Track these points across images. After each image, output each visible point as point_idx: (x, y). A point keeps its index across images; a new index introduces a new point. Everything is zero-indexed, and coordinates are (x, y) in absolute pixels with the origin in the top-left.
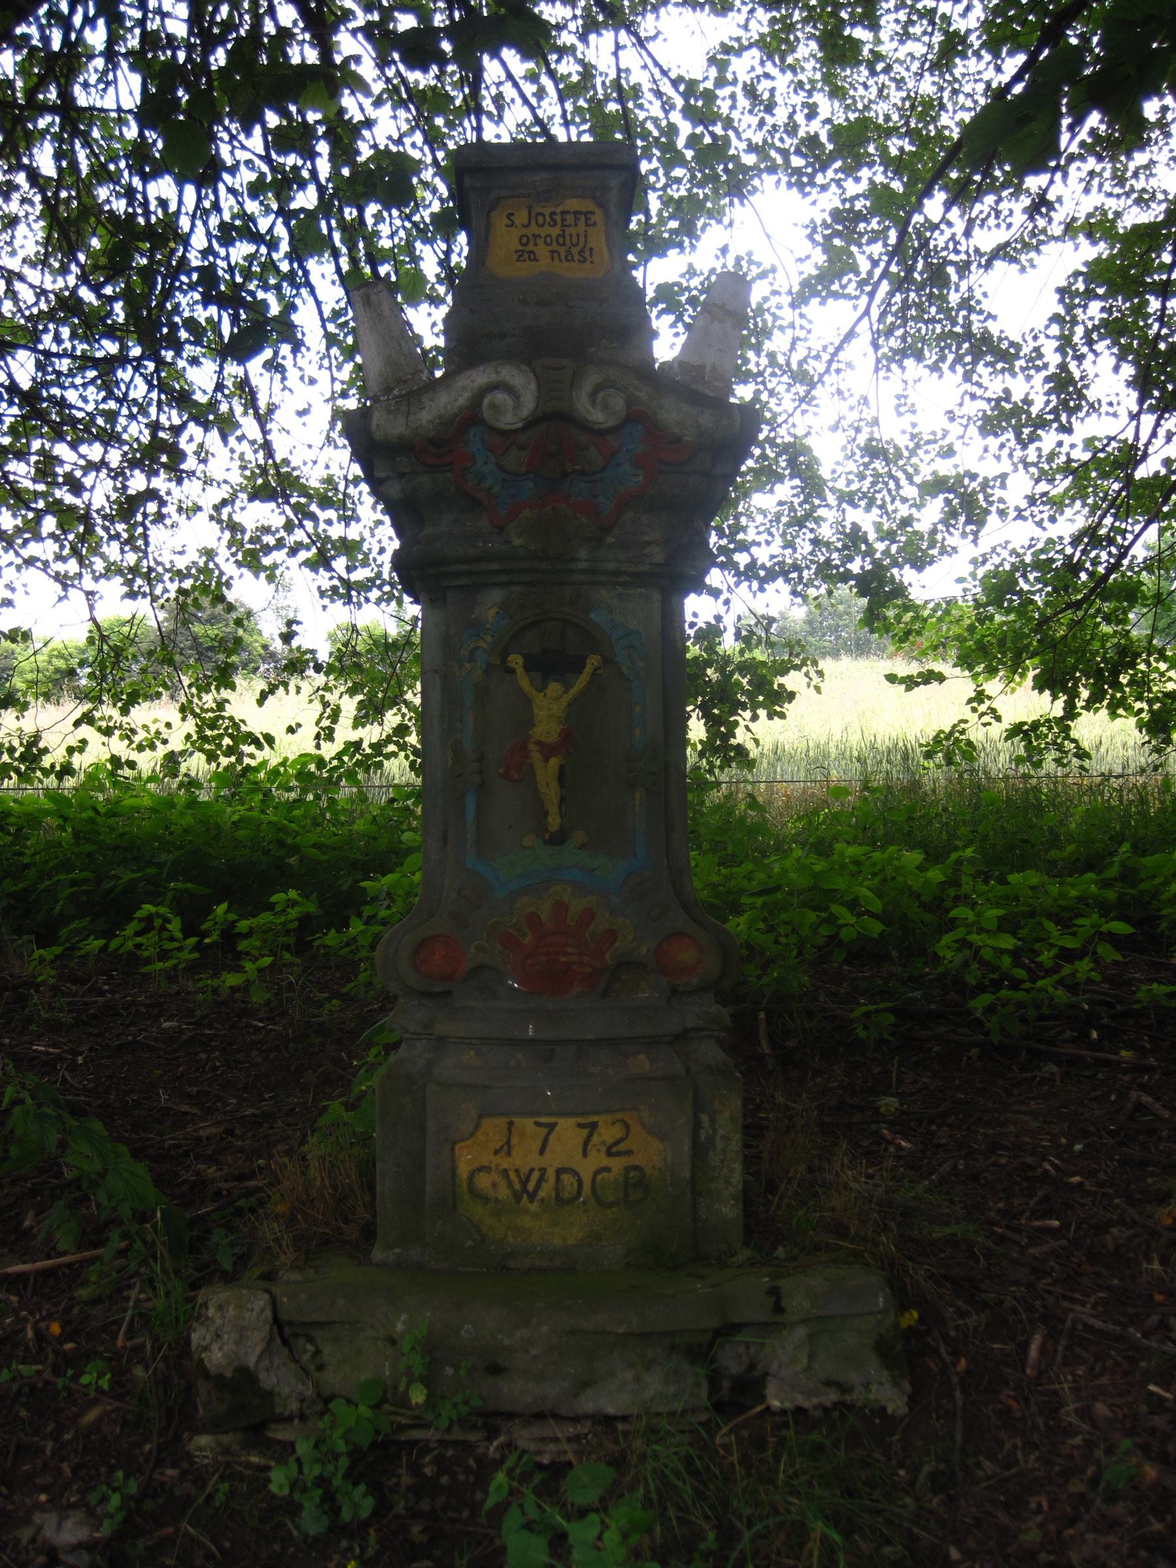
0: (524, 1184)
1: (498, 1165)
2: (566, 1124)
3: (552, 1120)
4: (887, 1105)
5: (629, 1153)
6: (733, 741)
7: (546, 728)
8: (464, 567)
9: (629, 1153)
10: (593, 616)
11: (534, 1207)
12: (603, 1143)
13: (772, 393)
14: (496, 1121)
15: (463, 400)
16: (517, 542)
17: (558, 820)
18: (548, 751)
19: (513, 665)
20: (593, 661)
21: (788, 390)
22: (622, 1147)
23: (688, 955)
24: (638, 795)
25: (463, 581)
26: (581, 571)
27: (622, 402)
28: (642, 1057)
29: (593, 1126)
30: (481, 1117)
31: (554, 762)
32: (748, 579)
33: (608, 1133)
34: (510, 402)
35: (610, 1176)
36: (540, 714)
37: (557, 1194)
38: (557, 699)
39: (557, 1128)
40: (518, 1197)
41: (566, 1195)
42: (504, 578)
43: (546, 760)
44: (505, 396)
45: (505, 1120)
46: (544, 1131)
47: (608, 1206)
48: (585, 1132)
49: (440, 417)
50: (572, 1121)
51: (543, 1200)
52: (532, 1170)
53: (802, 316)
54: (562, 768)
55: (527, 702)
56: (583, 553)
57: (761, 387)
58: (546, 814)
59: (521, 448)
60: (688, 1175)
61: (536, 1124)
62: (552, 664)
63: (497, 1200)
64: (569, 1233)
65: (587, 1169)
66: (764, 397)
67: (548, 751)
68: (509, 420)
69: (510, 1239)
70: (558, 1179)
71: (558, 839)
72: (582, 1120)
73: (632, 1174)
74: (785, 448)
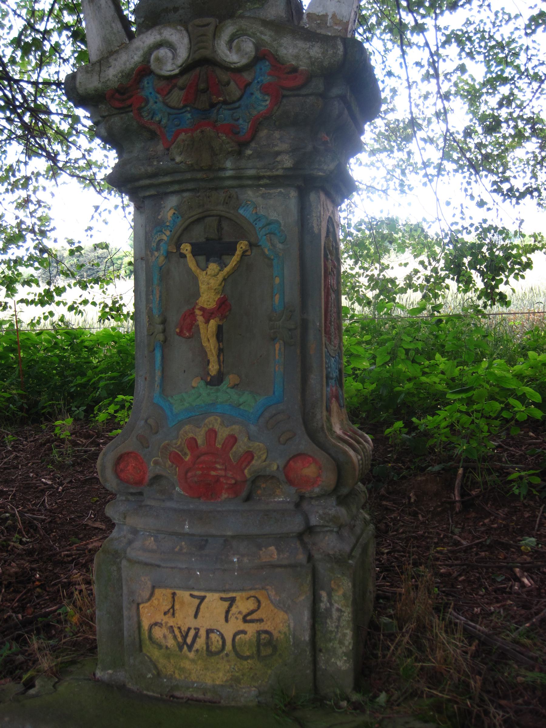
0: (185, 637)
1: (166, 623)
2: (212, 598)
3: (202, 594)
4: (526, 545)
5: (261, 620)
6: (497, 291)
7: (208, 299)
8: (147, 182)
9: (261, 620)
10: (241, 211)
11: (192, 655)
12: (240, 613)
13: (520, 90)
14: (164, 591)
15: (137, 58)
16: (178, 159)
17: (216, 367)
18: (208, 315)
19: (184, 252)
20: (242, 246)
21: (528, 87)
22: (254, 616)
23: (310, 471)
24: (277, 346)
25: (152, 192)
26: (229, 178)
27: (251, 45)
28: (272, 548)
29: (232, 600)
30: (154, 588)
31: (213, 323)
32: (510, 197)
33: (244, 605)
34: (170, 54)
35: (246, 637)
36: (203, 287)
37: (208, 647)
38: (215, 276)
39: (206, 600)
40: (181, 648)
41: (213, 649)
42: (176, 187)
43: (207, 322)
44: (167, 50)
45: (170, 591)
46: (197, 601)
47: (246, 658)
48: (226, 604)
49: (122, 72)
50: (217, 595)
51: (197, 651)
52: (189, 629)
53: (534, 42)
54: (220, 328)
55: (195, 279)
56: (228, 164)
57: (513, 86)
58: (208, 362)
59: (181, 89)
60: (307, 638)
61: (191, 595)
62: (212, 250)
63: (167, 647)
64: (214, 676)
65: (228, 630)
66: (516, 91)
67: (208, 315)
68: (170, 68)
69: (177, 675)
70: (208, 637)
71: (216, 381)
72: (224, 595)
73: (263, 636)
74: (529, 121)
